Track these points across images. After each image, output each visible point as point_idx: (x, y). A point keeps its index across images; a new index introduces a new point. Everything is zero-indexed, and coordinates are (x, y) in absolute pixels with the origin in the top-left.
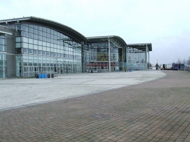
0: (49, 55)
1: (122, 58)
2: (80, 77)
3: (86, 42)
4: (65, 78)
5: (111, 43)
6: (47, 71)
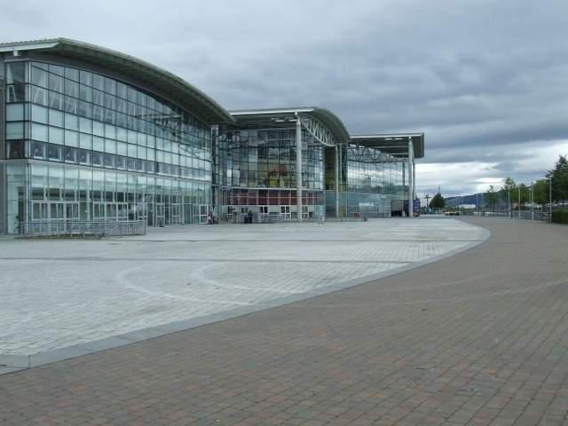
0: (75, 162)
1: (334, 179)
2: (229, 236)
3: (224, 127)
4: (172, 239)
5: (304, 130)
6: (106, 218)
